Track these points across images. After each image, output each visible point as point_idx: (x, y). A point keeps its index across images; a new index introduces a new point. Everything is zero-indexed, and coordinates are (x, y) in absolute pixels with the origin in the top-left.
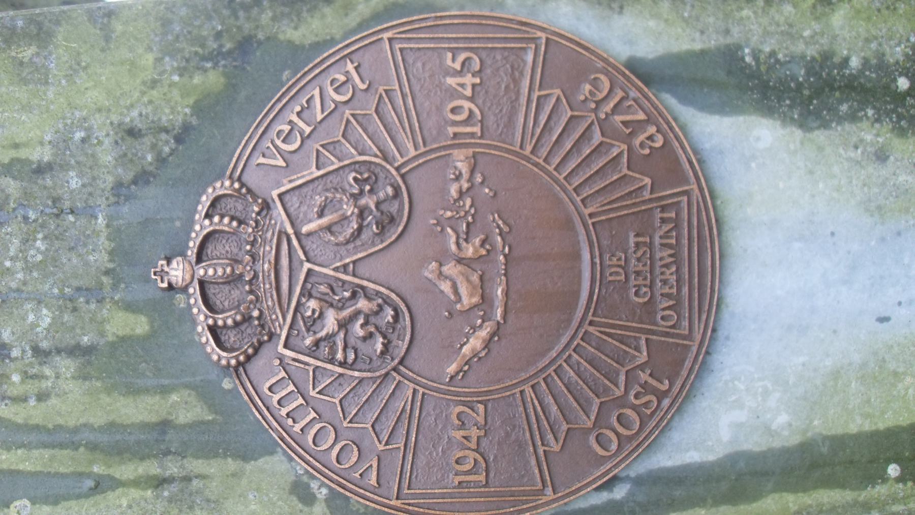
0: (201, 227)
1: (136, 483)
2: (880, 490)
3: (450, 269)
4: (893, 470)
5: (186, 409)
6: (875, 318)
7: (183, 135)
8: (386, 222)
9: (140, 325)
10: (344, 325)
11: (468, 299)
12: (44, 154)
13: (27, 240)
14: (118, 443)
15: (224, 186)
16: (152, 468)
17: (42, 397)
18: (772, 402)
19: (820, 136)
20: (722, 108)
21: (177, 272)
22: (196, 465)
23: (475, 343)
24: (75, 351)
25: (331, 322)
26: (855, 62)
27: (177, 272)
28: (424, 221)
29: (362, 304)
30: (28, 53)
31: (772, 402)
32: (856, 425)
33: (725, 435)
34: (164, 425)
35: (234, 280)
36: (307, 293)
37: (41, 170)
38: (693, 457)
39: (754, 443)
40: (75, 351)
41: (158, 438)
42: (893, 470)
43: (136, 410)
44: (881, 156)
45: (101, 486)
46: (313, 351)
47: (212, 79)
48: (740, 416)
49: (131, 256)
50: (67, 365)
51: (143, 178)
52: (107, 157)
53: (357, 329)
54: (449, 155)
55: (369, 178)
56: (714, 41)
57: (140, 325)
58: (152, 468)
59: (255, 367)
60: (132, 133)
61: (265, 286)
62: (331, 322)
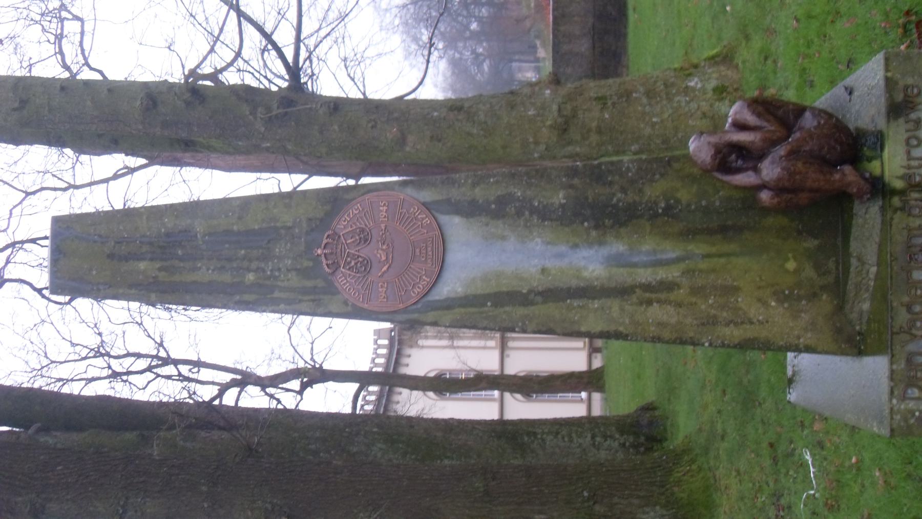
0: (325, 241)
1: (309, 301)
2: (486, 309)
3: (380, 251)
4: (489, 304)
5: (320, 283)
6: (34, 266)
7: (321, 220)
8: (366, 241)
9: (311, 264)
10: (356, 264)
11: (384, 258)
12: (289, 224)
13: (286, 244)
14: (305, 291)
15: (330, 232)
16: (312, 297)
17: (288, 280)
18: (458, 285)
19: (471, 220)
20: (448, 213)
21: (319, 251)
22: (322, 297)
23: (385, 268)
24: (296, 270)
25: (353, 263)
26: (481, 201)
27: (319, 251)
28: (374, 240)
29: (360, 259)
30: (287, 201)
31: (458, 285)
32: (479, 292)
33: (445, 293)
34: (315, 287)
35: (332, 253)
36: (348, 256)
37: (290, 228)
38: (437, 298)
39: (452, 295)
40: (296, 270)
41: (314, 290)
42: (489, 304)
43: (309, 284)
44: (487, 225)
45: (300, 301)
46: (349, 269)
47: (328, 207)
48: (449, 288)
49: (310, 247)
50: (294, 273)
51: (312, 230)
52: (304, 225)
53: (359, 265)
54: (320, 300)
55: (363, 230)
56: (444, 197)
57: (311, 264)
58: (312, 297)
59: (337, 273)
60: (310, 220)
61: (339, 254)
62: (353, 263)
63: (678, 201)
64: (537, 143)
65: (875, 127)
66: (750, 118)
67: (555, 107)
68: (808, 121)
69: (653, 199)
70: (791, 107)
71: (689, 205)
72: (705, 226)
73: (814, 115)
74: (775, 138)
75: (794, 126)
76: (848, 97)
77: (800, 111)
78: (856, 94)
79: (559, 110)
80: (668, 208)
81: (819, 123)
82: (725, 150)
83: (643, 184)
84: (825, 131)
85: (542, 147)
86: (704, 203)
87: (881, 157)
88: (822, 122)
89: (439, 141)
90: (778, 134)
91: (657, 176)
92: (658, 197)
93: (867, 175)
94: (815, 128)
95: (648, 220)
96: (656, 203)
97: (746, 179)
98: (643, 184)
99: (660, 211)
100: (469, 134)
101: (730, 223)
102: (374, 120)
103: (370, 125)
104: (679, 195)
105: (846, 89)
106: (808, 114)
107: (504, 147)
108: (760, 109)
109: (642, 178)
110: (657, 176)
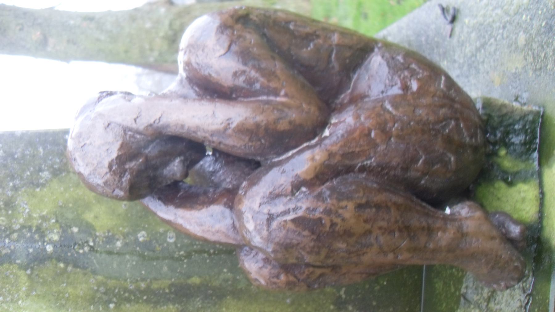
63: (88, 229)
64: (152, 50)
65: (328, 17)
66: (222, 65)
67: (167, 22)
68: (377, 79)
69: (35, 223)
70: (335, 38)
71: (110, 239)
72: (143, 285)
73: (395, 68)
74: (283, 126)
75: (341, 87)
76: (449, 27)
77: (360, 50)
78: (466, 21)
79: (171, 25)
80: (67, 243)
81: (406, 88)
82: (152, 151)
83: (15, 189)
84: (421, 112)
85: (156, 54)
86: (142, 236)
87: (540, 175)
88: (414, 86)
89: (75, 44)
90: (293, 115)
91: (46, 174)
92: (44, 218)
93: (515, 230)
94: (395, 101)
95: (24, 267)
96: (41, 232)
97: (205, 221)
98: (15, 189)
99: (49, 248)
100: (98, 40)
101: (196, 280)
102: (22, 24)
103: (18, 28)
104: (89, 217)
105: (444, 10)
106: (376, 62)
107: (126, 52)
108: (251, 38)
109: (13, 178)
110: (46, 174)
